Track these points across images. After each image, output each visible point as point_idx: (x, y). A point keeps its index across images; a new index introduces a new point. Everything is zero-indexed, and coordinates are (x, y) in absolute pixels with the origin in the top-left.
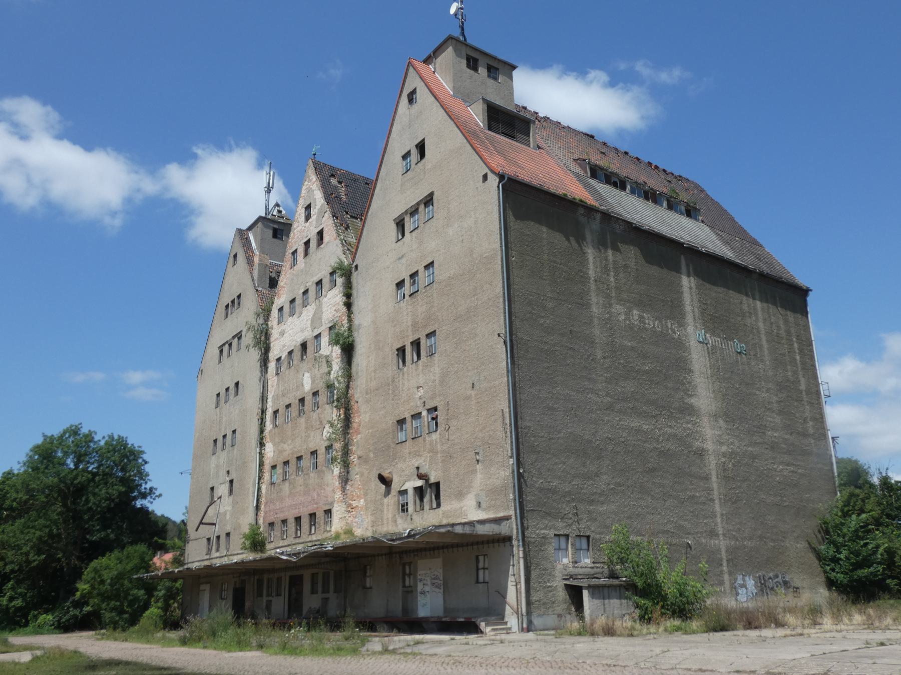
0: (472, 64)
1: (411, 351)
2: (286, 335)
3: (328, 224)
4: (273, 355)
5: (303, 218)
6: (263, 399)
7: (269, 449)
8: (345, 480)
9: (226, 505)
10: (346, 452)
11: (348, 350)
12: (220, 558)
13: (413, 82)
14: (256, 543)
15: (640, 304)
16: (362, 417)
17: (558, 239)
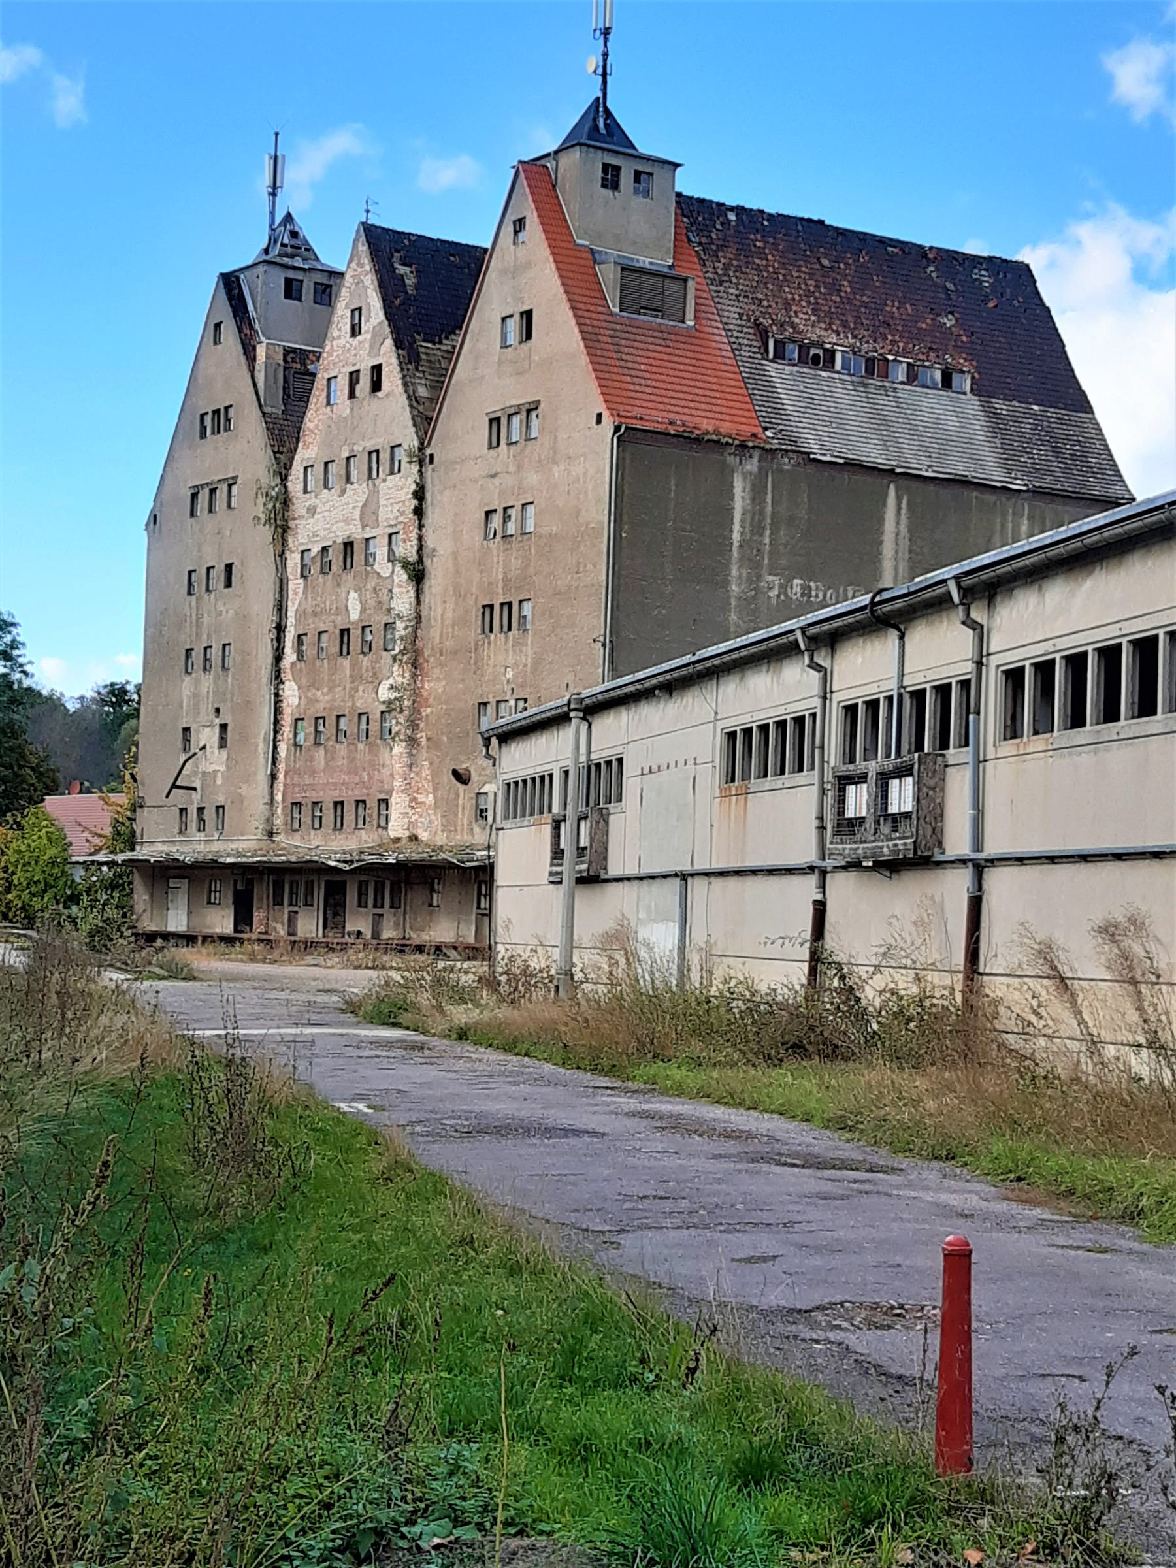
2: (323, 518)
6: (281, 607)
7: (291, 692)
9: (215, 761)
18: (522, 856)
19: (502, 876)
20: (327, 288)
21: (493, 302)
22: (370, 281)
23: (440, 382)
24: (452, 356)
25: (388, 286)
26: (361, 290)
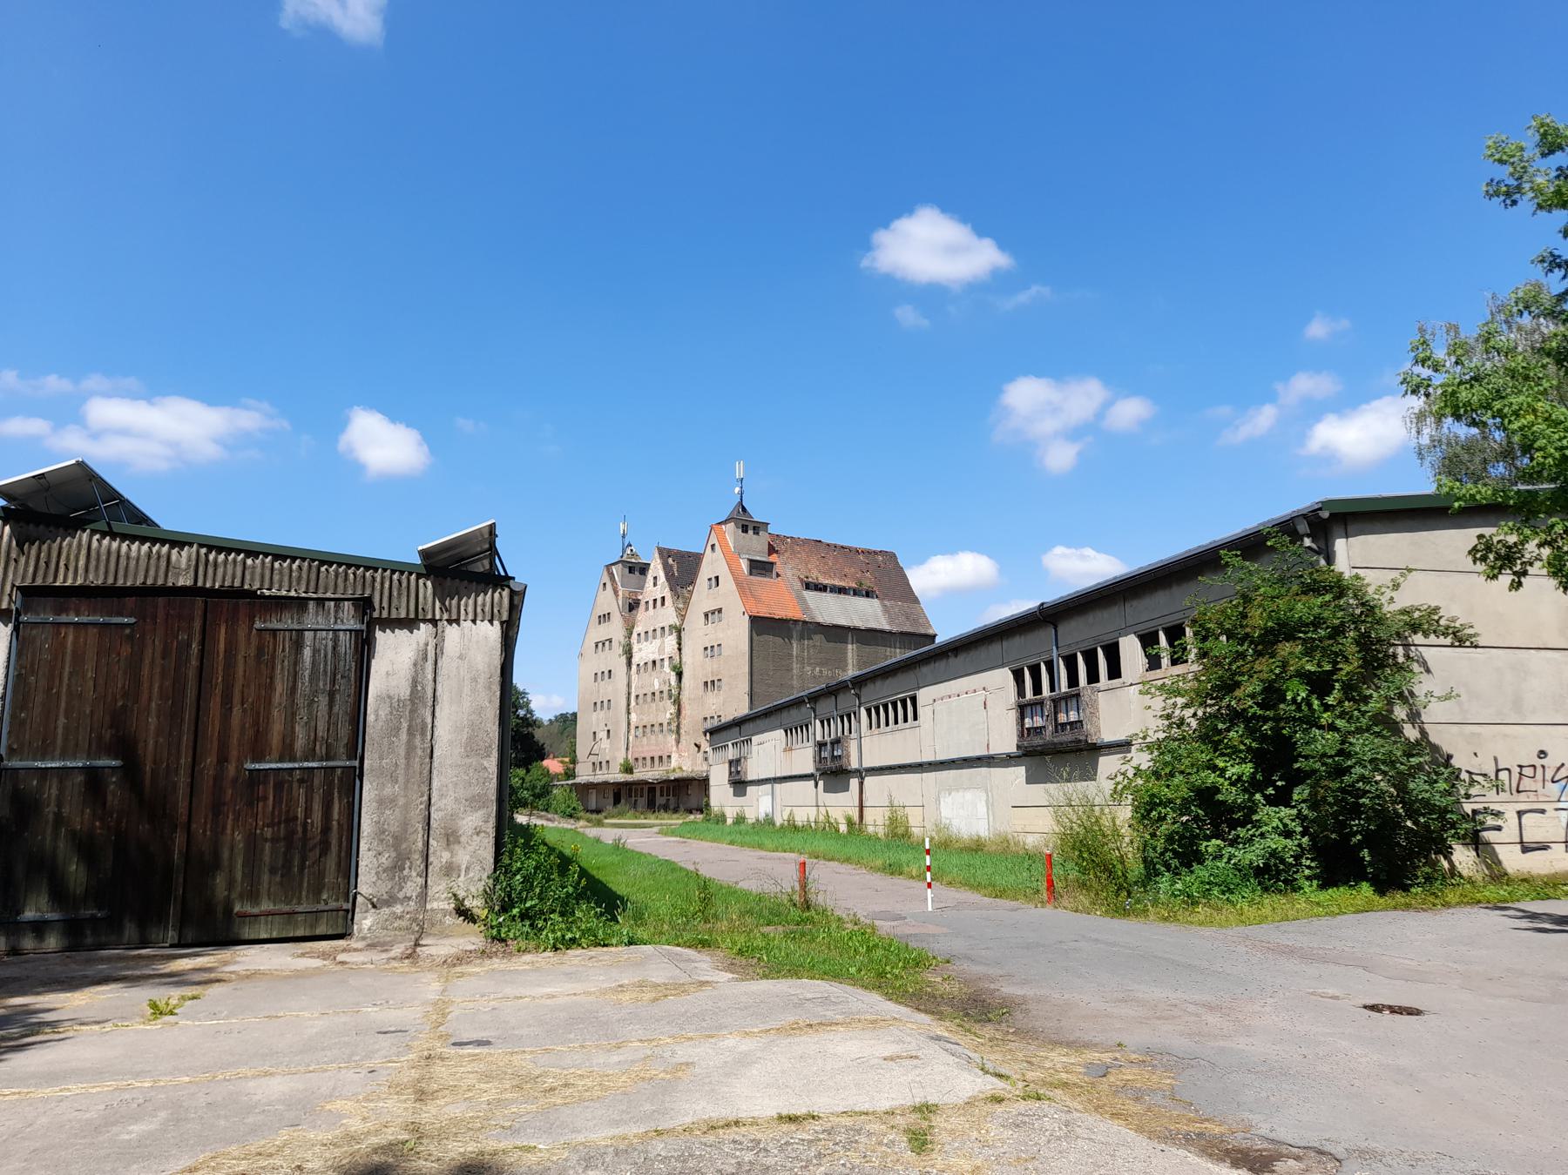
0: (745, 529)
1: (710, 685)
2: (645, 652)
3: (667, 593)
4: (635, 660)
5: (886, 1054)
6: (629, 685)
7: (633, 716)
8: (678, 742)
9: (605, 744)
10: (678, 727)
11: (680, 675)
12: (600, 777)
13: (714, 540)
14: (628, 769)
15: (821, 664)
16: (686, 712)
17: (779, 640)
18: (719, 779)
19: (712, 782)
20: (643, 569)
21: (705, 572)
22: (660, 567)
23: (687, 602)
24: (691, 592)
25: (667, 568)
26: (656, 568)
